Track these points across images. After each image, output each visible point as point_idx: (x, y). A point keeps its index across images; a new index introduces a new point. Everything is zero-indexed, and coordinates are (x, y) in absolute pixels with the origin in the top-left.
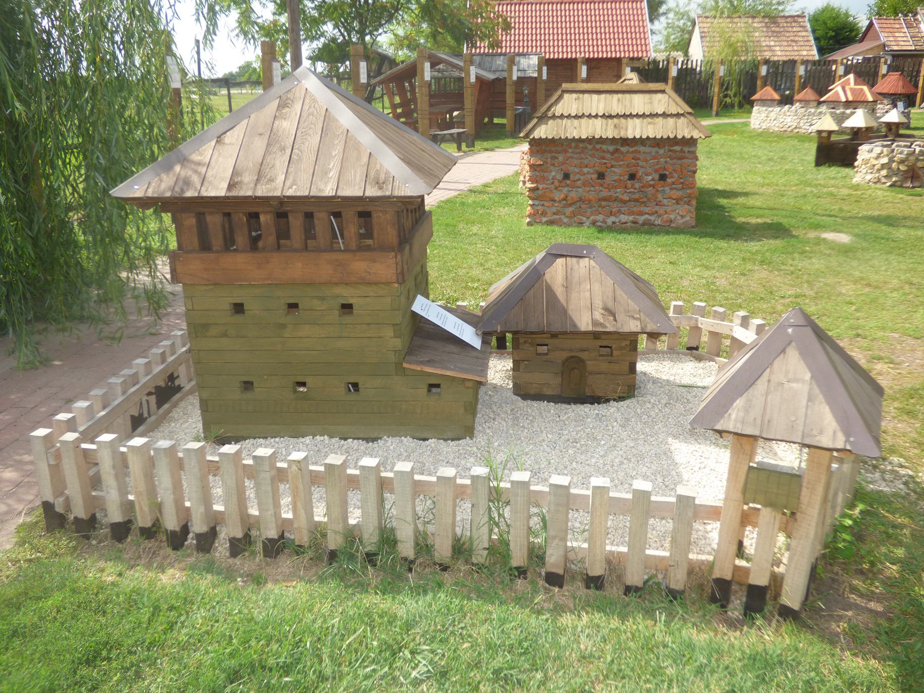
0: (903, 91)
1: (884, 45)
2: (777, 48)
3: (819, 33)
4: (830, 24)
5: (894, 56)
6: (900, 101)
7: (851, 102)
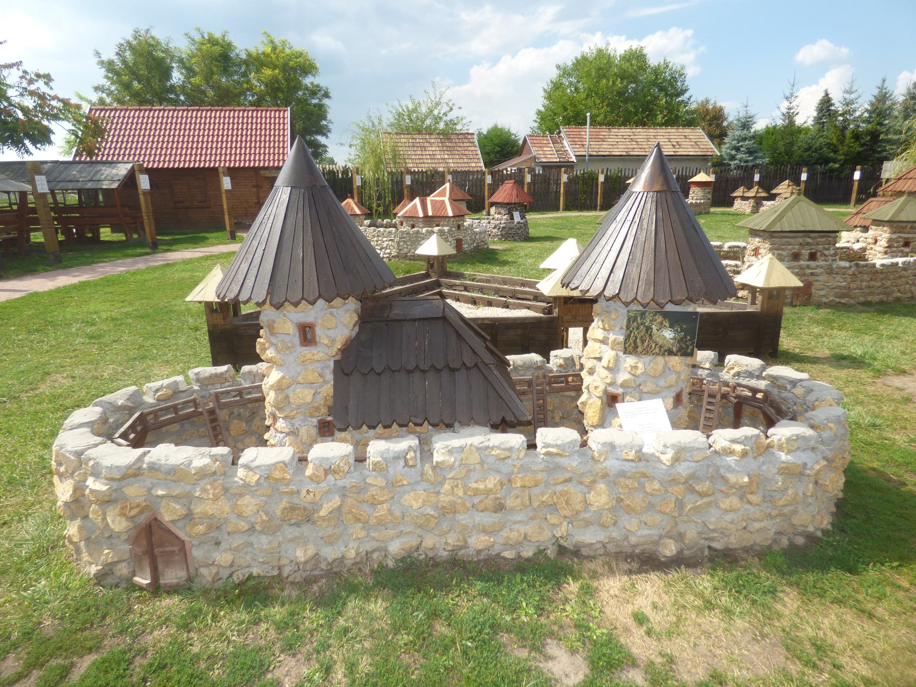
0: (517, 201)
1: (535, 158)
2: (451, 161)
3: (487, 149)
4: (496, 141)
5: (543, 167)
6: (517, 210)
7: (432, 217)
